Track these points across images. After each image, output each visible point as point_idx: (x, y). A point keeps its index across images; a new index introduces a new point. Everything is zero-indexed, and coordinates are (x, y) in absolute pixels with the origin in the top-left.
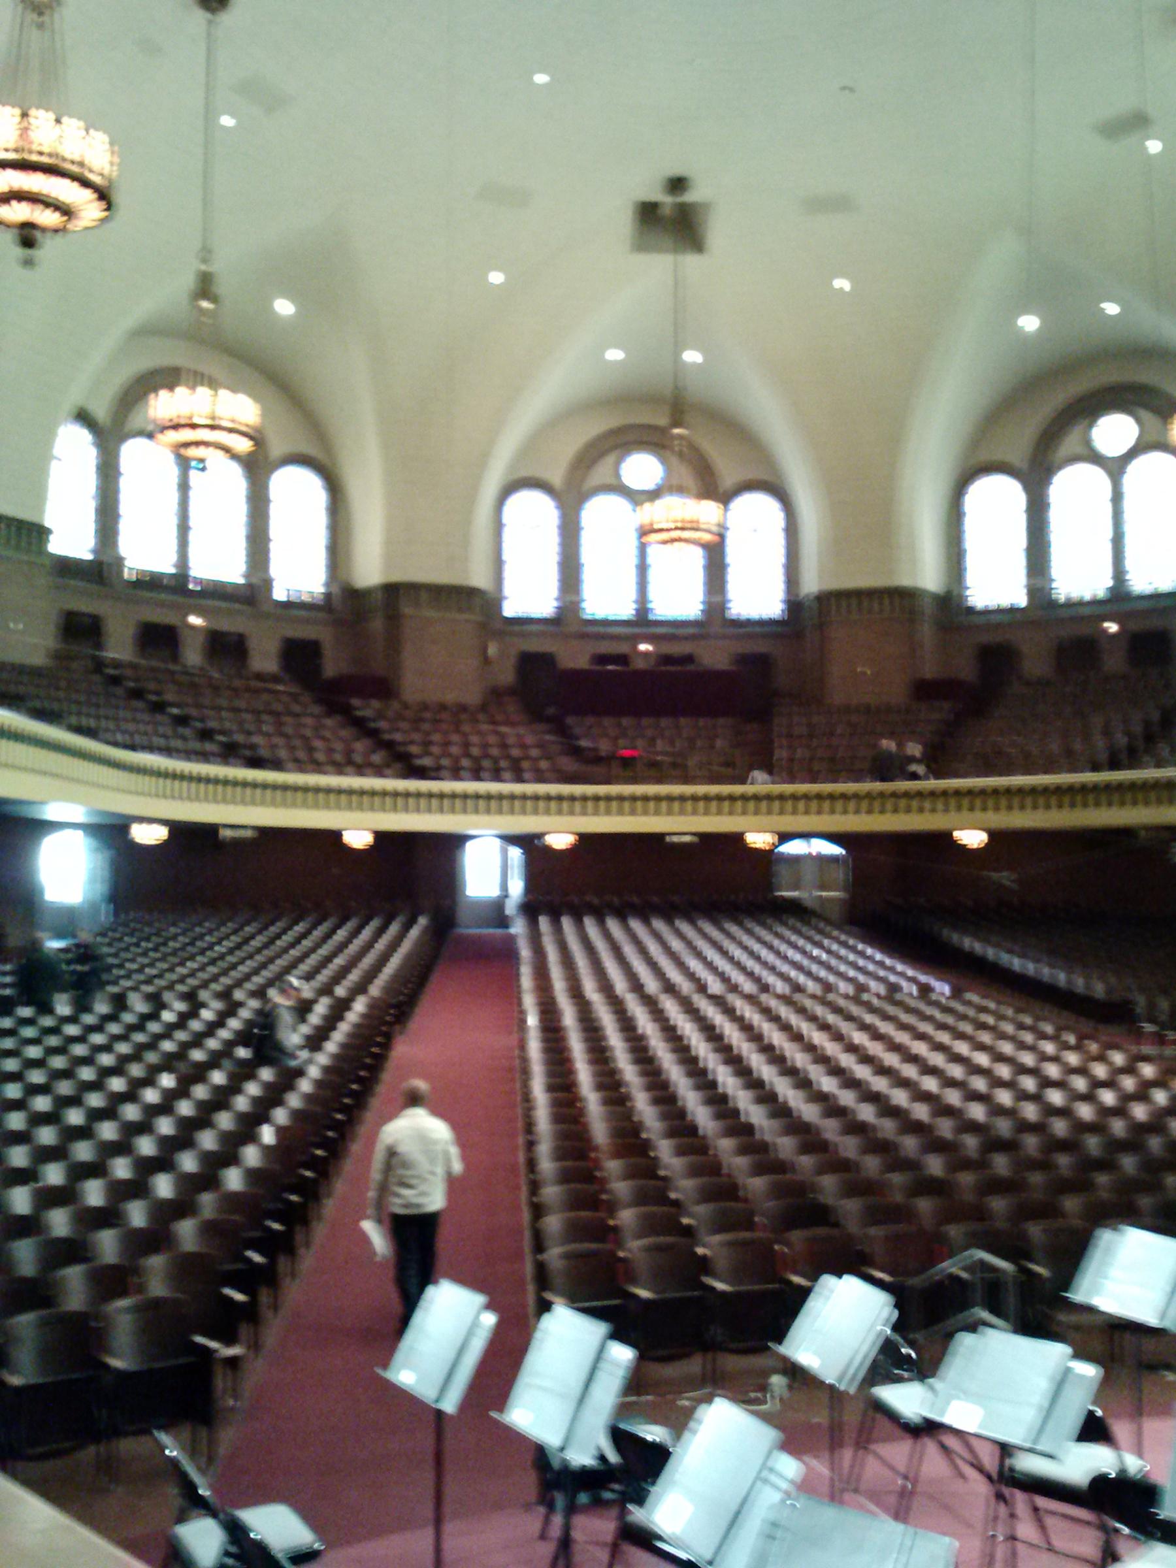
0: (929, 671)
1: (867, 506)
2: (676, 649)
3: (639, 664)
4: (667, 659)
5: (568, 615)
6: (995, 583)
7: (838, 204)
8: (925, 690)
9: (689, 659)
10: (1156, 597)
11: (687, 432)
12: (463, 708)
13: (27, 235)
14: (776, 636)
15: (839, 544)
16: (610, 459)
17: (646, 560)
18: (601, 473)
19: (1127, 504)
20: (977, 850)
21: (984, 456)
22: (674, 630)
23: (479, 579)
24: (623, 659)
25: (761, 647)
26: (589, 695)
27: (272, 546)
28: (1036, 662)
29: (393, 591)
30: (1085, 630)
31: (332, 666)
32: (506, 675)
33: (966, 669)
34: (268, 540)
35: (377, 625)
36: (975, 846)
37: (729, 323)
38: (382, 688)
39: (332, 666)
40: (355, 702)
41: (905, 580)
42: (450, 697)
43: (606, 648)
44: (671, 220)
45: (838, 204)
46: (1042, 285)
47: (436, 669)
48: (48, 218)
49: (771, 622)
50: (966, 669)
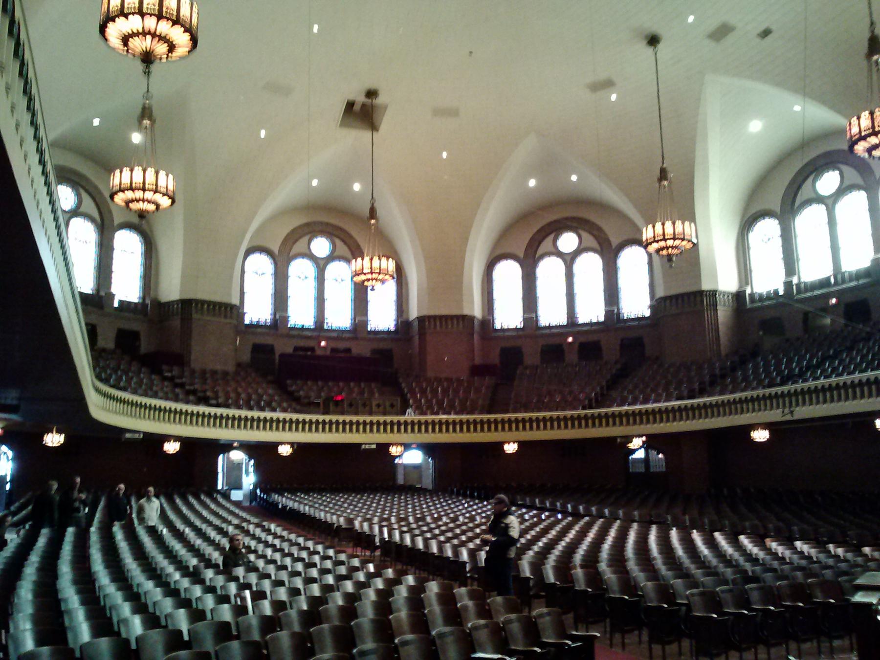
0: (478, 361)
1: (446, 270)
2: (341, 345)
3: (319, 352)
4: (333, 350)
5: (279, 321)
6: (508, 315)
7: (452, 113)
8: (478, 371)
9: (348, 350)
10: (591, 324)
11: (347, 227)
12: (225, 374)
13: (147, 58)
14: (602, 331)
15: (431, 290)
16: (305, 239)
17: (324, 295)
18: (300, 246)
19: (576, 280)
20: (172, 454)
21: (499, 252)
22: (338, 335)
23: (235, 301)
24: (312, 349)
25: (382, 345)
26: (293, 366)
27: (113, 275)
28: (531, 357)
29: (187, 305)
30: (557, 341)
31: (145, 346)
32: (246, 357)
33: (495, 358)
34: (111, 272)
35: (176, 323)
36: (285, 454)
37: (387, 170)
38: (180, 360)
39: (145, 346)
40: (164, 367)
41: (466, 312)
42: (219, 367)
43: (302, 343)
44: (363, 113)
45: (452, 113)
46: (546, 164)
47: (210, 351)
48: (161, 49)
49: (388, 332)
50: (495, 358)
